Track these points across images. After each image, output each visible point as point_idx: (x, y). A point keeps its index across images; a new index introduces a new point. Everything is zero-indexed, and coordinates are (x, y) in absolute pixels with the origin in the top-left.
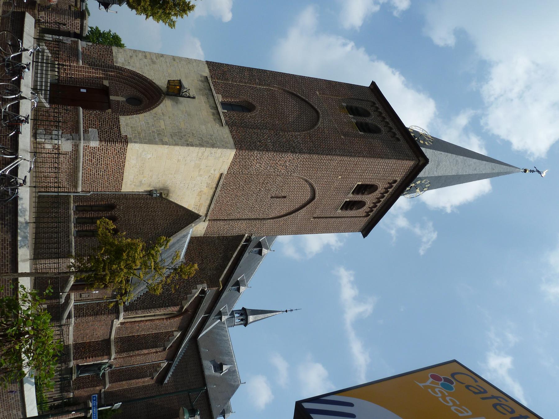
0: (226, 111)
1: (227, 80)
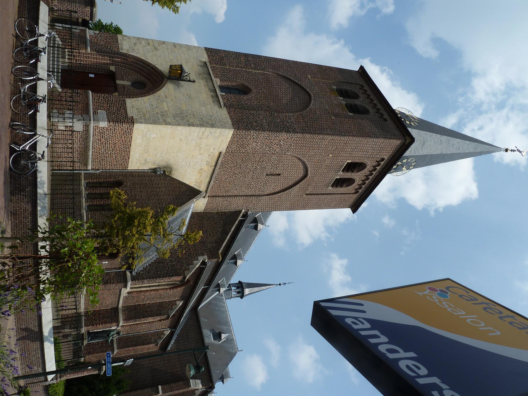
0: (224, 94)
1: (225, 65)
